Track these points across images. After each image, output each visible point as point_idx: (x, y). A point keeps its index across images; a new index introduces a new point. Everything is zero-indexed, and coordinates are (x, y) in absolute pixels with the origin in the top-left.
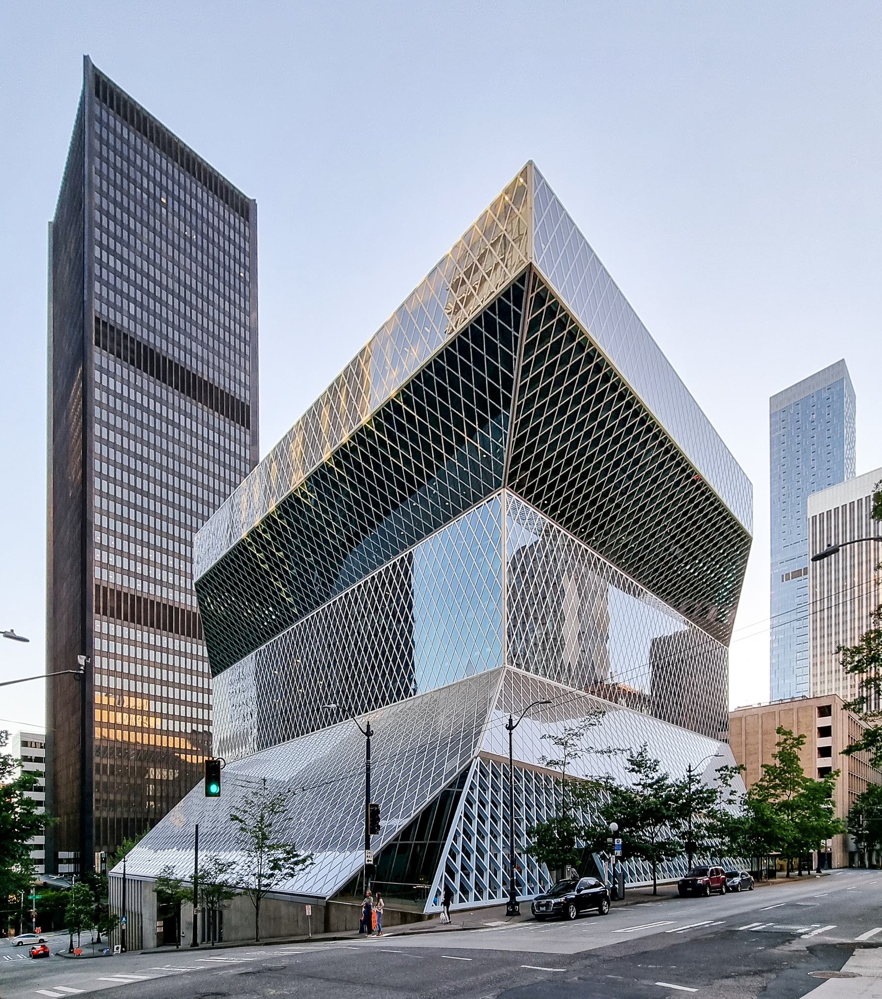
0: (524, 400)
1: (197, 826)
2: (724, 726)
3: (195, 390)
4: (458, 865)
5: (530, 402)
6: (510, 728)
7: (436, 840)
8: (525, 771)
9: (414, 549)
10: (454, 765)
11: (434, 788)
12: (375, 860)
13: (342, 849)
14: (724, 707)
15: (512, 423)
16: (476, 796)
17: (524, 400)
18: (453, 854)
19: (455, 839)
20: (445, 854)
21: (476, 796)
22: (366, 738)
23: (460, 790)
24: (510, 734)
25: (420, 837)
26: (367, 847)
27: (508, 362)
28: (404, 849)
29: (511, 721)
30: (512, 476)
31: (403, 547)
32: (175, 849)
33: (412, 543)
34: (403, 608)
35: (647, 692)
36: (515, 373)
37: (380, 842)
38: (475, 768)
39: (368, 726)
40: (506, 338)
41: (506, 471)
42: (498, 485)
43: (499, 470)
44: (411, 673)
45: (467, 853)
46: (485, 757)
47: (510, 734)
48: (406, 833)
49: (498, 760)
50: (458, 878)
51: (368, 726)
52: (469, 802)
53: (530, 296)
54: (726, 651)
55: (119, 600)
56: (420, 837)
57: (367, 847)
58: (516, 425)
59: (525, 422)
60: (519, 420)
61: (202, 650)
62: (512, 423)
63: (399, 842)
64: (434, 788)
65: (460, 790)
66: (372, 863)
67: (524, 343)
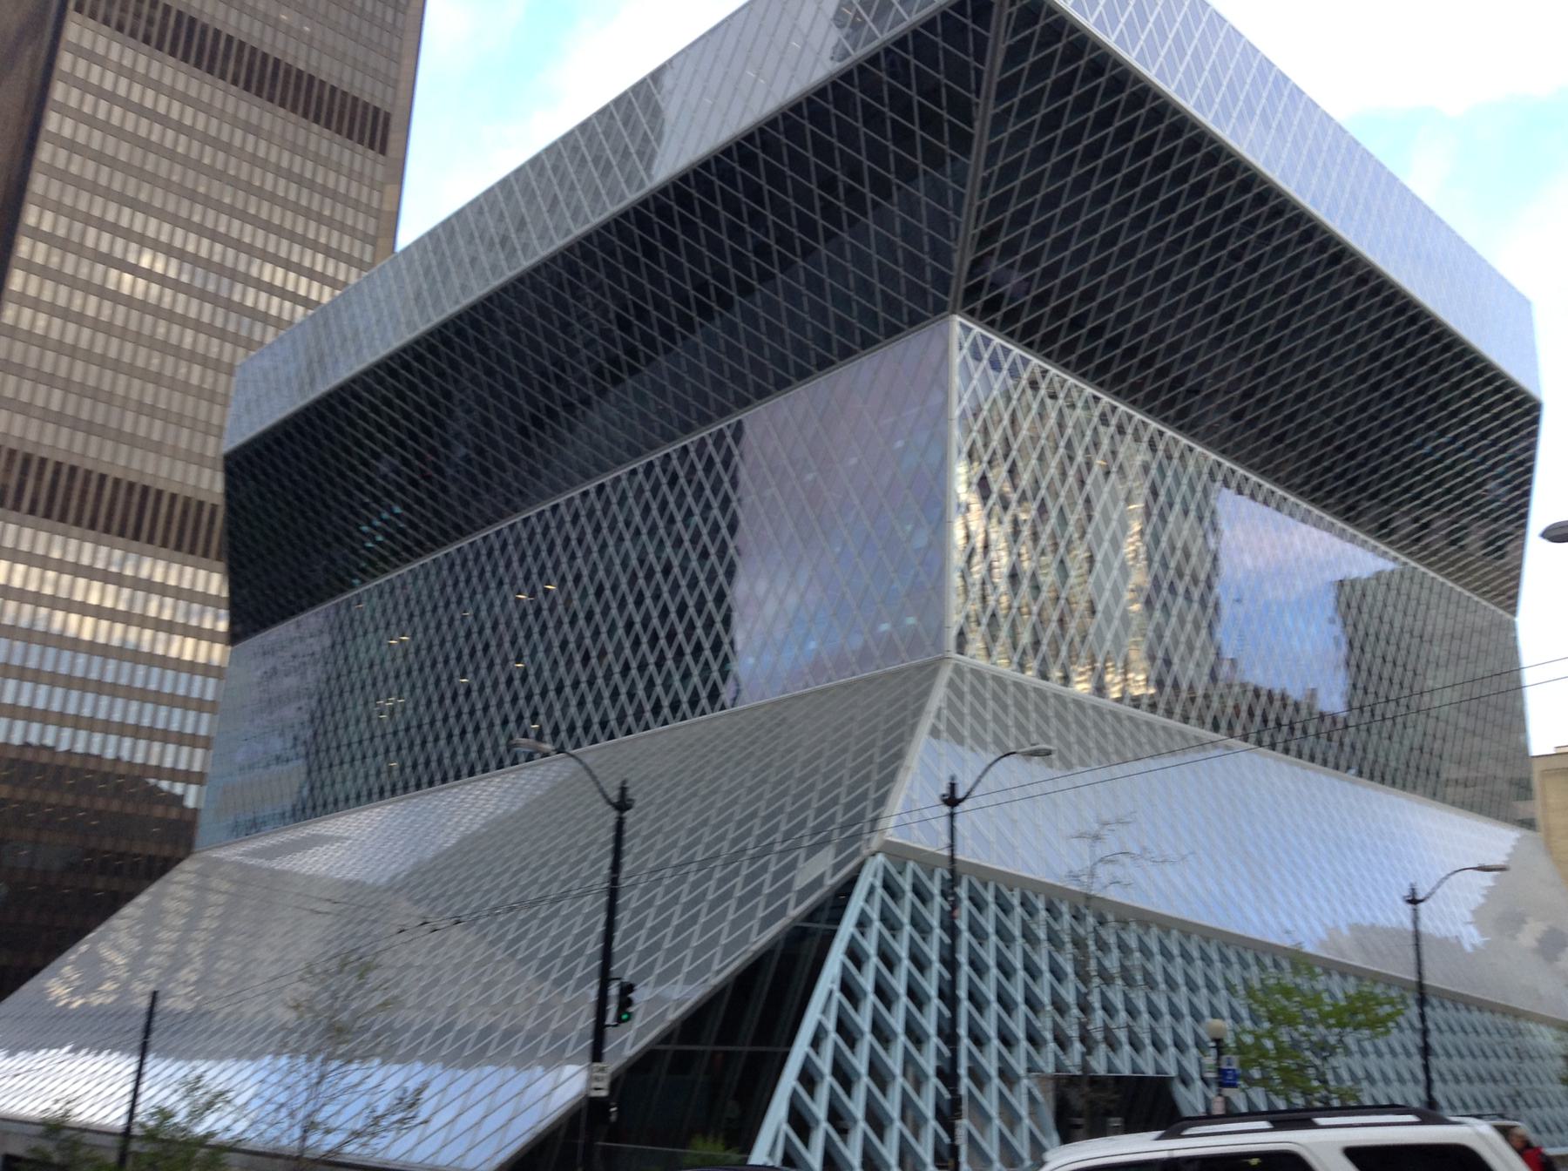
0: (996, 168)
1: (154, 996)
2: (1523, 789)
3: (273, 86)
4: (820, 1109)
5: (1009, 172)
6: (952, 800)
7: (697, 1042)
8: (997, 889)
9: (745, 416)
10: (820, 868)
11: (766, 923)
12: (614, 1084)
13: (524, 1062)
14: (1523, 749)
15: (971, 205)
16: (870, 946)
17: (996, 168)
18: (808, 1078)
19: (816, 1043)
20: (789, 1080)
21: (870, 946)
22: (614, 814)
23: (832, 927)
24: (952, 816)
25: (728, 1033)
26: (597, 1054)
27: (963, 110)
28: (682, 1063)
29: (953, 786)
30: (972, 293)
31: (724, 412)
32: (67, 1049)
33: (744, 403)
34: (716, 529)
35: (1333, 700)
36: (977, 124)
37: (627, 1044)
38: (870, 879)
39: (623, 790)
40: (959, 72)
41: (959, 284)
42: (940, 309)
43: (943, 282)
44: (726, 660)
45: (844, 1076)
46: (898, 855)
47: (952, 816)
48: (694, 1023)
49: (927, 862)
50: (818, 1140)
51: (623, 790)
52: (855, 955)
53: (1007, 11)
54: (1511, 628)
55: (24, 472)
56: (728, 1033)
57: (597, 1054)
58: (980, 209)
59: (999, 204)
60: (987, 200)
61: (215, 583)
62: (971, 205)
63: (672, 1047)
64: (766, 923)
65: (832, 927)
66: (604, 1093)
67: (996, 79)
